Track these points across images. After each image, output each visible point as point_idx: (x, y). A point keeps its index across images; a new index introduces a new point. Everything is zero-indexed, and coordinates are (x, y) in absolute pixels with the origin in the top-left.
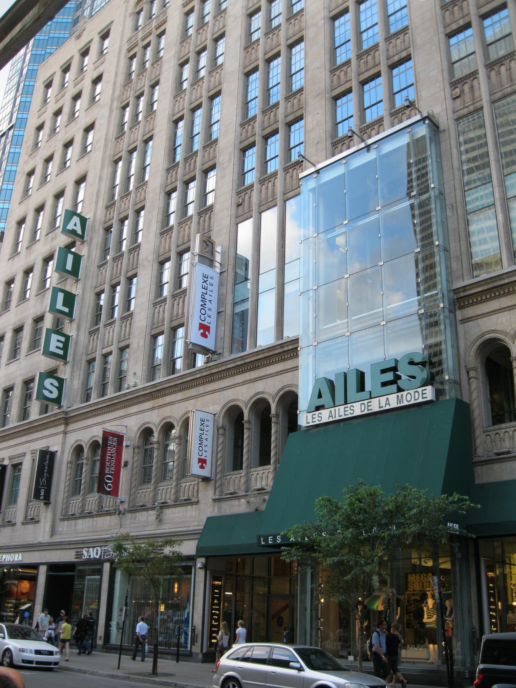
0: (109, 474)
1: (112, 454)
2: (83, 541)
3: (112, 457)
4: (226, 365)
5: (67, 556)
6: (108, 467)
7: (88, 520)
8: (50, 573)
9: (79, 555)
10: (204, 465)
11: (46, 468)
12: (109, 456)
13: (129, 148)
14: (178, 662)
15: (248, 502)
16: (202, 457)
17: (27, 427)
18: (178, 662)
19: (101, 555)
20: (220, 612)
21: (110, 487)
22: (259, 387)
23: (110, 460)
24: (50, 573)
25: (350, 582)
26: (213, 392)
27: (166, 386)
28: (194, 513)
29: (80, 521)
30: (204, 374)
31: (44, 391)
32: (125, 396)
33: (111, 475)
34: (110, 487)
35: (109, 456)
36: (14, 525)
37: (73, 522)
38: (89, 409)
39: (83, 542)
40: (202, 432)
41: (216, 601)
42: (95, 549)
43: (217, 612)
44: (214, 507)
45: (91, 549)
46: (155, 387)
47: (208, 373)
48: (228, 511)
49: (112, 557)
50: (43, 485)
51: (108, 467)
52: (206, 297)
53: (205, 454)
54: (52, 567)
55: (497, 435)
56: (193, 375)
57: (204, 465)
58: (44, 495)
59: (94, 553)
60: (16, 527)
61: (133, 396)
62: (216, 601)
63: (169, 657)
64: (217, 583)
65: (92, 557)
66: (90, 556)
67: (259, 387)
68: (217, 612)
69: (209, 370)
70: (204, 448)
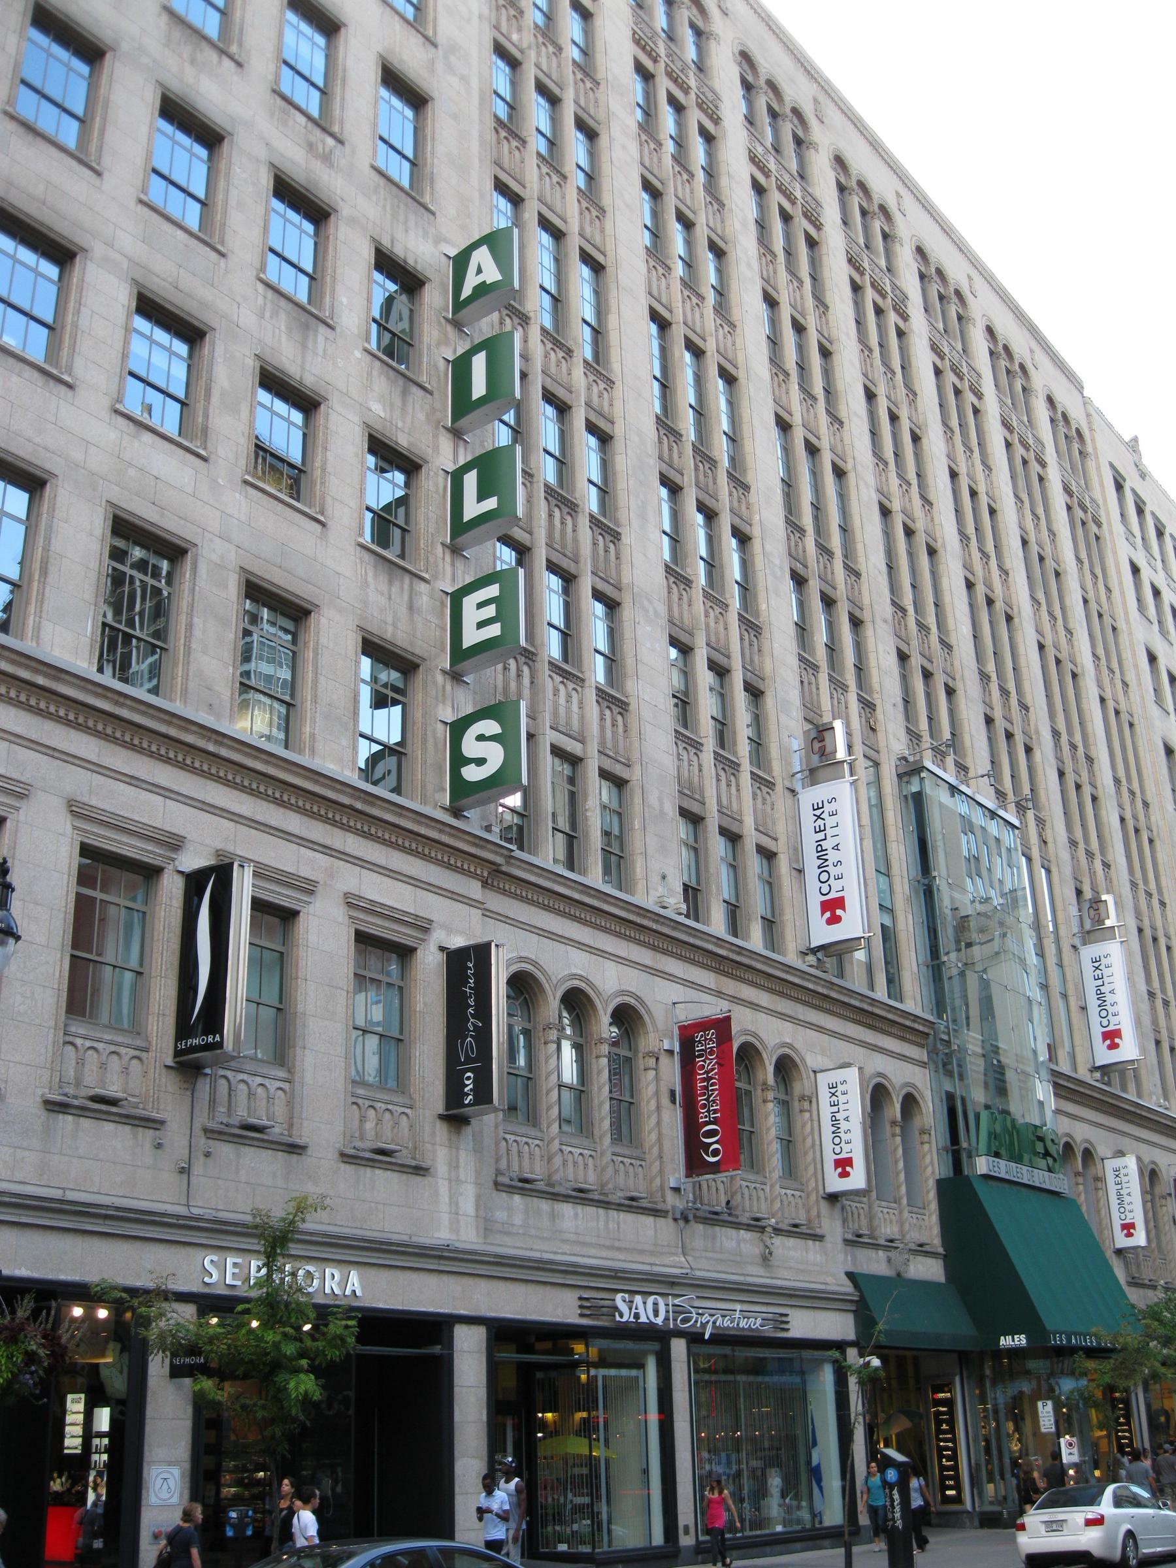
0: (710, 1123)
1: (707, 1072)
2: (617, 1271)
3: (708, 1079)
4: (851, 997)
5: (558, 1307)
6: (704, 1106)
8: (437, 1349)
9: (781, 1322)
10: (848, 1169)
11: (471, 1002)
12: (703, 1080)
15: (889, 1260)
16: (843, 1155)
17: (345, 800)
19: (667, 1319)
20: (938, 1445)
21: (715, 1153)
23: (706, 1088)
24: (437, 1349)
25: (324, 1406)
26: (820, 1029)
27: (759, 966)
28: (818, 1258)
30: (820, 990)
32: (674, 929)
34: (715, 1153)
35: (703, 1080)
37: (545, 1206)
38: (577, 896)
39: (615, 1274)
40: (835, 1109)
41: (944, 1427)
42: (651, 1299)
43: (950, 1444)
44: (846, 1255)
45: (638, 1299)
46: (739, 954)
47: (825, 991)
48: (865, 1267)
49: (694, 1325)
50: (469, 1060)
51: (704, 1106)
52: (825, 844)
53: (846, 1148)
54: (504, 1334)
55: (115, 1057)
56: (803, 979)
57: (848, 1169)
59: (646, 1310)
60: (308, 1161)
61: (691, 940)
62: (1122, 1420)
63: (827, 1542)
64: (941, 1395)
65: (643, 1319)
66: (637, 1316)
68: (950, 1444)
69: (828, 988)
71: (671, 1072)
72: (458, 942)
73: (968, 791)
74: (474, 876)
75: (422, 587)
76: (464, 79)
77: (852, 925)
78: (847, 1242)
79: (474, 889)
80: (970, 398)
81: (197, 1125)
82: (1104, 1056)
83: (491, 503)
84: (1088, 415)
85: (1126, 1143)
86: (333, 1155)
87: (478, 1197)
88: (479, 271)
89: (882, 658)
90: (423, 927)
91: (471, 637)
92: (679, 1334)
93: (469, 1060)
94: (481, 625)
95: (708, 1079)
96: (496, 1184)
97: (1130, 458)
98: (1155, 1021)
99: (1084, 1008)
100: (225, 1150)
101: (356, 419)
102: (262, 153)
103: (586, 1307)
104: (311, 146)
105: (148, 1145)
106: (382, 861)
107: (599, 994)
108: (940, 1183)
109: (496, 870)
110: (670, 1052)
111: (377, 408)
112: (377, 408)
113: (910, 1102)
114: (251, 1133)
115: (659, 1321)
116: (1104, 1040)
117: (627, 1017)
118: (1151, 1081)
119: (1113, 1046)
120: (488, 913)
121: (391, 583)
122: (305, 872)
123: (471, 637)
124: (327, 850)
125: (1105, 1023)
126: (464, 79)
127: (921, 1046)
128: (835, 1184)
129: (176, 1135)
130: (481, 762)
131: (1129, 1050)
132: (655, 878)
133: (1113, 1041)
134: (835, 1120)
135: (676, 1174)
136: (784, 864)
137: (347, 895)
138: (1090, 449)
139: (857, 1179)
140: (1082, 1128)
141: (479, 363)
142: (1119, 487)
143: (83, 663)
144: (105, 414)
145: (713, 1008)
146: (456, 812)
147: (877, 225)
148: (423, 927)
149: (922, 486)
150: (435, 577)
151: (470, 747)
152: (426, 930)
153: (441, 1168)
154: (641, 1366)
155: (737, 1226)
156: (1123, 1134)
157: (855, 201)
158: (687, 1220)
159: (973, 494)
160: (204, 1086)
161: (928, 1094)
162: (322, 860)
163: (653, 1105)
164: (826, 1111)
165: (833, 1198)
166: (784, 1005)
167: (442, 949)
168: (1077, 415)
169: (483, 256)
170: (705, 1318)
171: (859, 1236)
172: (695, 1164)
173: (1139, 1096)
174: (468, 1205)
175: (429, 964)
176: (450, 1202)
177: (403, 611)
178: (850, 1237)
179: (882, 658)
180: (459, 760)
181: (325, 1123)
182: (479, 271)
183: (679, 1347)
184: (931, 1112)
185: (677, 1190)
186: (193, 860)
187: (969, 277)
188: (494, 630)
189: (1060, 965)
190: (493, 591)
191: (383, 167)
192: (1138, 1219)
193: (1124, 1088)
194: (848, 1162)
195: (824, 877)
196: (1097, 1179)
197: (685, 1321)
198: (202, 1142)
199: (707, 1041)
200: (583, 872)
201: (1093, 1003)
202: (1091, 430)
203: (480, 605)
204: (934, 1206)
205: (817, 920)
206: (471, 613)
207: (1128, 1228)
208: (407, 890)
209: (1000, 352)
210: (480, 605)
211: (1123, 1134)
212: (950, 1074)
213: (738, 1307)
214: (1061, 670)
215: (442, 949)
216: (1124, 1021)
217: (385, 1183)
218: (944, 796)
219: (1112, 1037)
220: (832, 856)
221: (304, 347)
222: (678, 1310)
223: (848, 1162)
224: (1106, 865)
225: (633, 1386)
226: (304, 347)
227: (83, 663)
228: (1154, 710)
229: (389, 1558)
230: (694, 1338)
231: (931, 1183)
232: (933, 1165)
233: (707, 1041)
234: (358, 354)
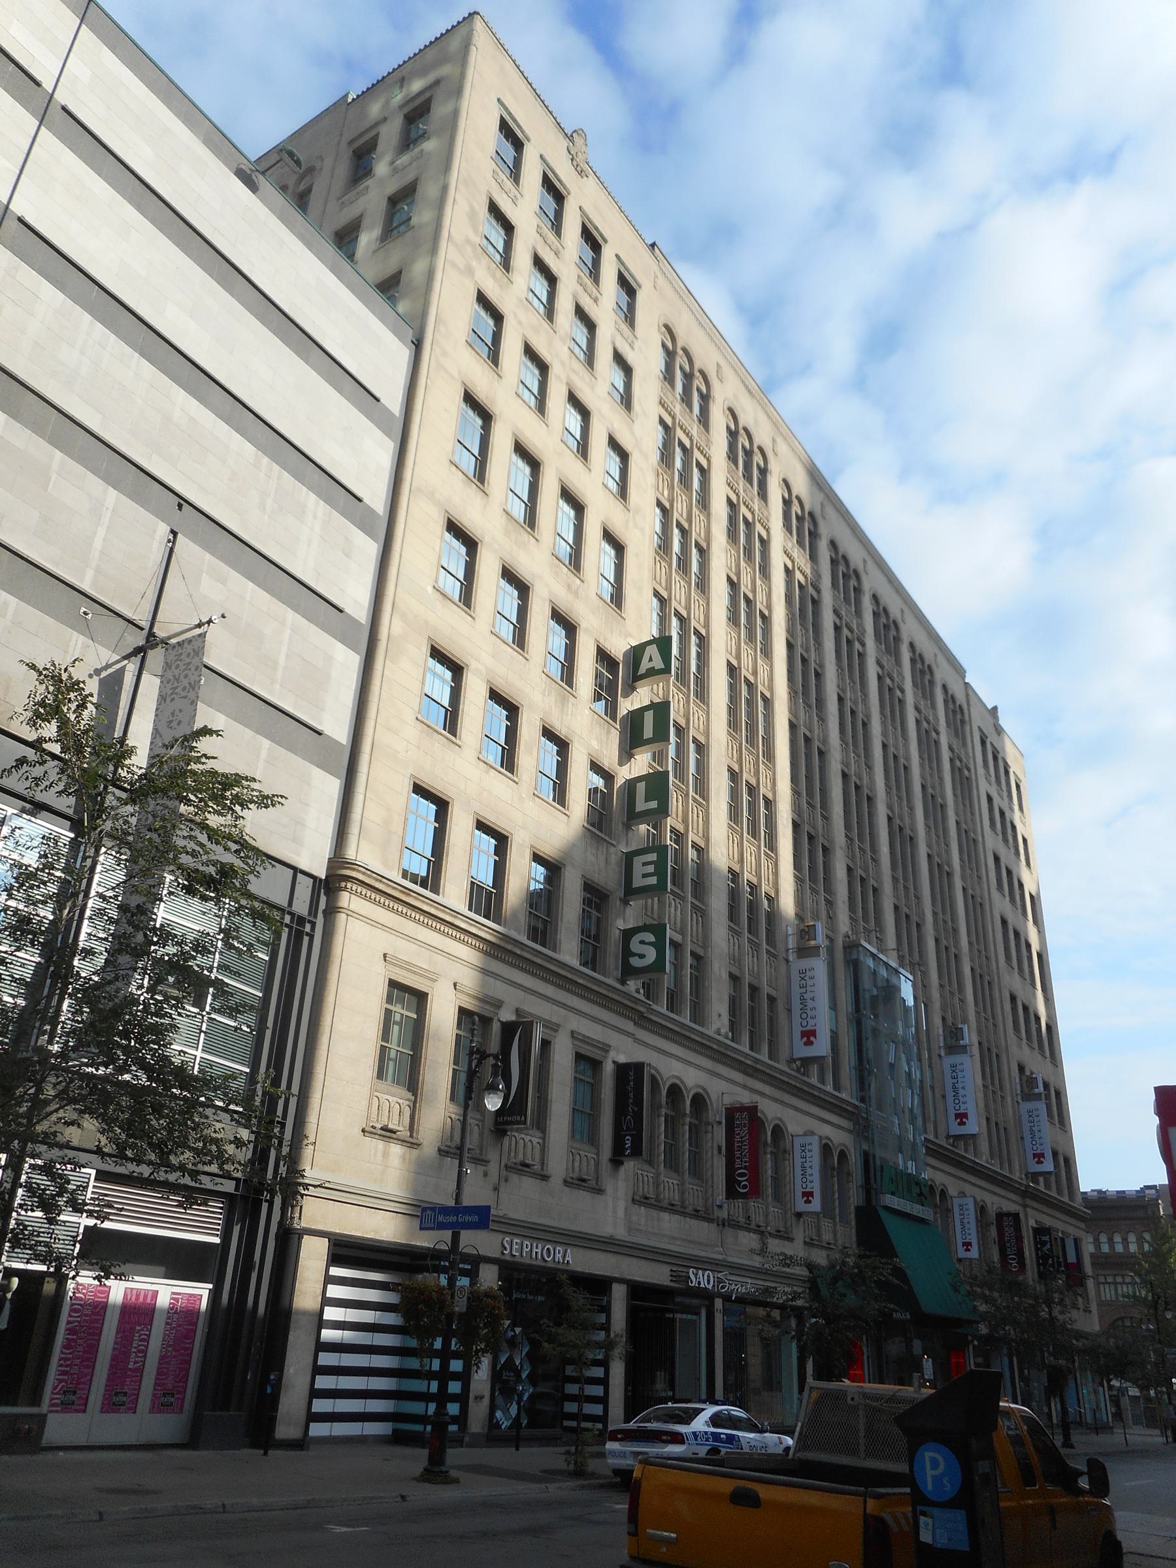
3: (742, 1142)
5: (658, 1275)
7: (677, 1217)
11: (631, 1095)
13: (681, 548)
14: (517, 1449)
18: (517, 1449)
21: (745, 1187)
22: (612, 1038)
26: (796, 1109)
29: (665, 1216)
31: (653, 939)
33: (745, 1168)
34: (745, 1187)
36: (545, 1178)
37: (654, 1213)
50: (628, 1129)
53: (810, 1185)
54: (637, 1290)
58: (632, 1147)
59: (702, 1279)
67: (612, 1038)
70: (809, 1178)
71: (720, 1135)
72: (622, 1059)
73: (884, 958)
74: (630, 1019)
75: (612, 849)
76: (642, 530)
77: (822, 1047)
78: (805, 1243)
79: (630, 1026)
80: (857, 645)
81: (503, 1164)
82: (956, 1130)
83: (653, 804)
84: (967, 695)
85: (968, 1189)
86: (560, 1181)
87: (626, 1209)
88: (651, 660)
89: (840, 873)
90: (606, 1048)
91: (638, 882)
92: (720, 1295)
93: (628, 1129)
94: (644, 876)
95: (742, 1142)
96: (633, 1200)
97: (991, 720)
98: (986, 1106)
99: (944, 1097)
100: (514, 1178)
101: (585, 752)
102: (546, 595)
103: (675, 1276)
104: (569, 587)
105: (481, 1174)
106: (589, 1011)
107: (686, 1088)
108: (858, 1209)
109: (641, 1016)
110: (720, 1123)
111: (594, 744)
112: (594, 744)
113: (843, 1155)
114: (523, 1168)
115: (710, 1287)
116: (802, 1037)
117: (699, 1101)
118: (984, 1146)
119: (809, 1043)
120: (637, 1041)
121: (598, 849)
122: (554, 1019)
123: (638, 882)
124: (564, 1006)
125: (804, 1023)
126: (642, 530)
127: (850, 1120)
128: (801, 1206)
129: (493, 1168)
130: (642, 956)
131: (973, 1126)
132: (715, 1016)
133: (809, 1039)
134: (803, 1168)
135: (720, 1196)
136: (780, 1006)
137: (572, 1032)
138: (967, 718)
139: (816, 1205)
140: (935, 1174)
141: (649, 717)
142: (983, 743)
143: (575, 963)
144: (474, 760)
145: (745, 1098)
146: (623, 982)
147: (853, 582)
148: (606, 1048)
149: (909, 800)
150: (618, 843)
151: (635, 946)
152: (607, 1051)
153: (609, 1189)
154: (698, 1314)
155: (749, 1230)
156: (965, 1181)
157: (842, 568)
158: (724, 1225)
159: (853, 712)
160: (506, 1140)
161: (852, 1151)
162: (563, 1012)
163: (710, 1154)
164: (798, 1161)
165: (799, 1215)
166: (778, 1094)
167: (614, 1062)
168: (960, 697)
169: (652, 650)
170: (733, 1287)
171: (646, 1198)
172: (732, 1192)
173: (1010, 1172)
174: (621, 1213)
175: (496, 1027)
176: (611, 1211)
177: (602, 864)
178: (807, 1240)
179: (840, 873)
180: (627, 953)
181: (558, 1164)
182: (651, 660)
183: (718, 1303)
184: (855, 1161)
185: (720, 1207)
186: (507, 1015)
187: (718, 365)
188: (653, 880)
189: (930, 1067)
190: (653, 857)
191: (509, 510)
192: (816, 1187)
193: (966, 1150)
194: (811, 1194)
195: (804, 1016)
196: (948, 1210)
197: (723, 1287)
198: (504, 1173)
199: (742, 1119)
200: (679, 1013)
201: (950, 1094)
202: (968, 704)
203: (644, 864)
204: (853, 1223)
205: (798, 1042)
206: (638, 869)
207: (967, 1245)
208: (599, 1028)
209: (880, 612)
210: (644, 864)
211: (965, 1181)
212: (866, 1139)
213: (749, 1281)
214: (941, 872)
215: (614, 1062)
216: (823, 1023)
217: (583, 1198)
218: (870, 963)
219: (962, 1117)
220: (961, 1092)
221: (562, 710)
222: (720, 1281)
223: (811, 1194)
224: (995, 1025)
225: (694, 1324)
226: (562, 710)
227: (575, 963)
228: (995, 895)
229: (720, 1412)
230: (727, 1298)
231: (853, 1207)
232: (855, 1198)
233: (742, 1119)
234: (587, 712)
